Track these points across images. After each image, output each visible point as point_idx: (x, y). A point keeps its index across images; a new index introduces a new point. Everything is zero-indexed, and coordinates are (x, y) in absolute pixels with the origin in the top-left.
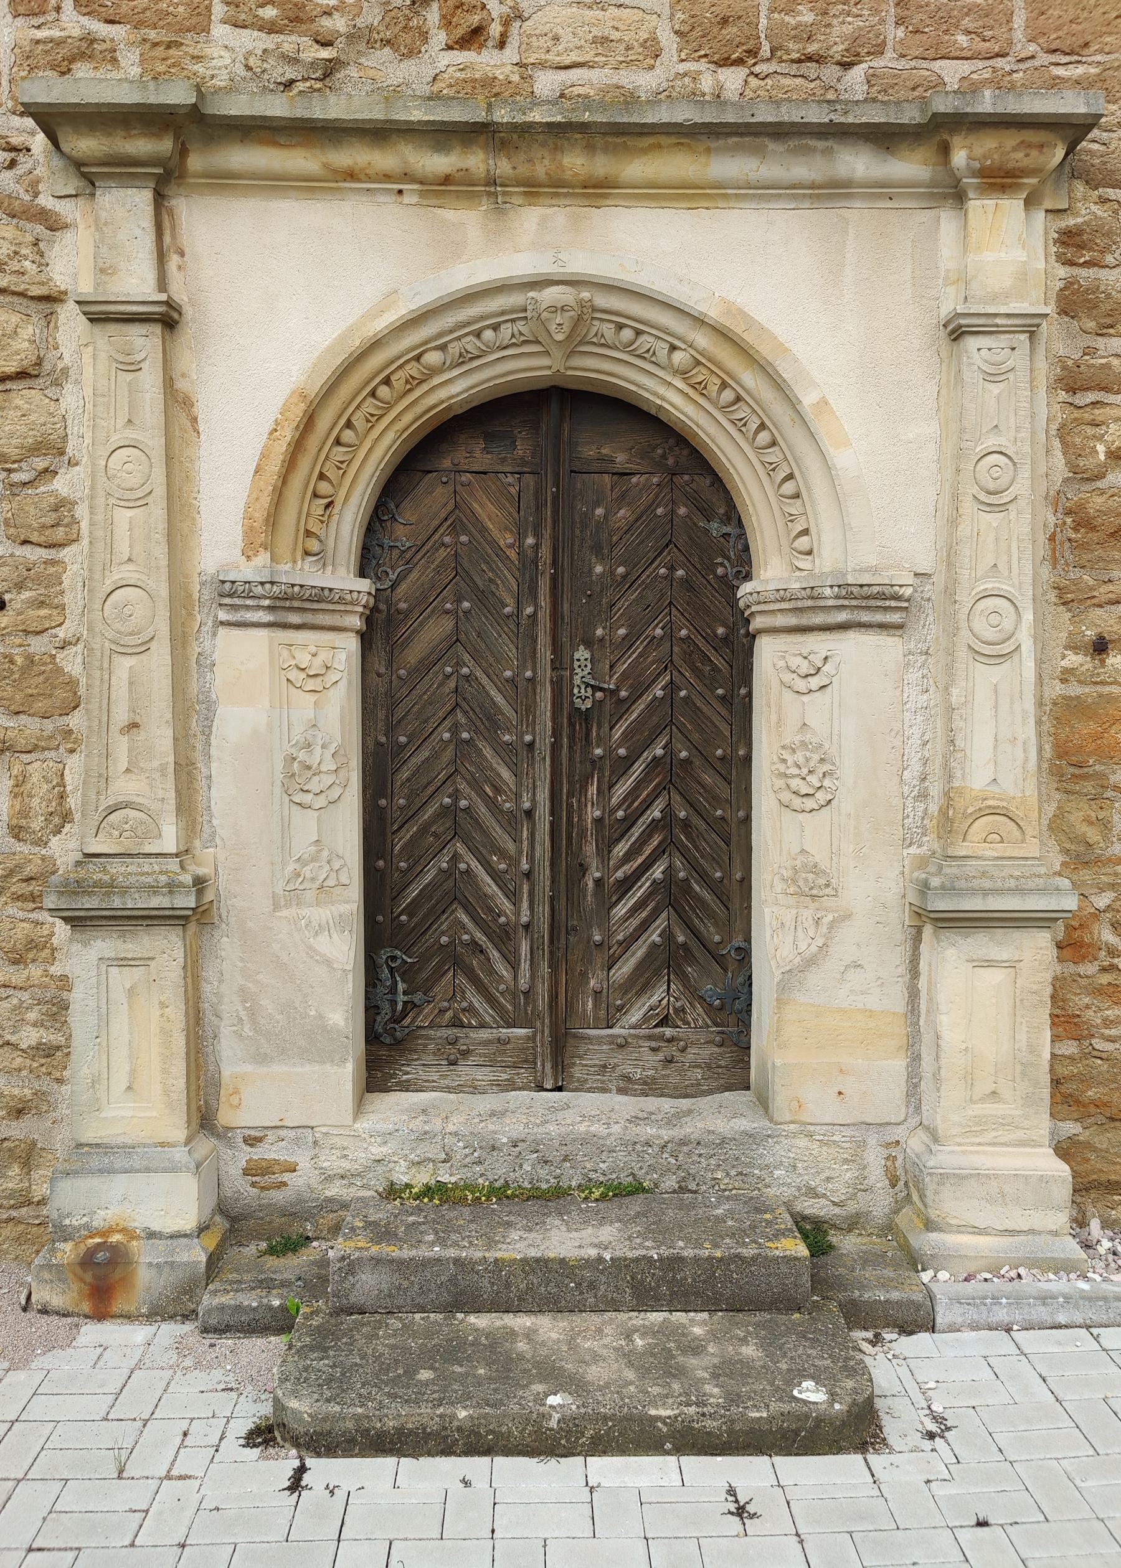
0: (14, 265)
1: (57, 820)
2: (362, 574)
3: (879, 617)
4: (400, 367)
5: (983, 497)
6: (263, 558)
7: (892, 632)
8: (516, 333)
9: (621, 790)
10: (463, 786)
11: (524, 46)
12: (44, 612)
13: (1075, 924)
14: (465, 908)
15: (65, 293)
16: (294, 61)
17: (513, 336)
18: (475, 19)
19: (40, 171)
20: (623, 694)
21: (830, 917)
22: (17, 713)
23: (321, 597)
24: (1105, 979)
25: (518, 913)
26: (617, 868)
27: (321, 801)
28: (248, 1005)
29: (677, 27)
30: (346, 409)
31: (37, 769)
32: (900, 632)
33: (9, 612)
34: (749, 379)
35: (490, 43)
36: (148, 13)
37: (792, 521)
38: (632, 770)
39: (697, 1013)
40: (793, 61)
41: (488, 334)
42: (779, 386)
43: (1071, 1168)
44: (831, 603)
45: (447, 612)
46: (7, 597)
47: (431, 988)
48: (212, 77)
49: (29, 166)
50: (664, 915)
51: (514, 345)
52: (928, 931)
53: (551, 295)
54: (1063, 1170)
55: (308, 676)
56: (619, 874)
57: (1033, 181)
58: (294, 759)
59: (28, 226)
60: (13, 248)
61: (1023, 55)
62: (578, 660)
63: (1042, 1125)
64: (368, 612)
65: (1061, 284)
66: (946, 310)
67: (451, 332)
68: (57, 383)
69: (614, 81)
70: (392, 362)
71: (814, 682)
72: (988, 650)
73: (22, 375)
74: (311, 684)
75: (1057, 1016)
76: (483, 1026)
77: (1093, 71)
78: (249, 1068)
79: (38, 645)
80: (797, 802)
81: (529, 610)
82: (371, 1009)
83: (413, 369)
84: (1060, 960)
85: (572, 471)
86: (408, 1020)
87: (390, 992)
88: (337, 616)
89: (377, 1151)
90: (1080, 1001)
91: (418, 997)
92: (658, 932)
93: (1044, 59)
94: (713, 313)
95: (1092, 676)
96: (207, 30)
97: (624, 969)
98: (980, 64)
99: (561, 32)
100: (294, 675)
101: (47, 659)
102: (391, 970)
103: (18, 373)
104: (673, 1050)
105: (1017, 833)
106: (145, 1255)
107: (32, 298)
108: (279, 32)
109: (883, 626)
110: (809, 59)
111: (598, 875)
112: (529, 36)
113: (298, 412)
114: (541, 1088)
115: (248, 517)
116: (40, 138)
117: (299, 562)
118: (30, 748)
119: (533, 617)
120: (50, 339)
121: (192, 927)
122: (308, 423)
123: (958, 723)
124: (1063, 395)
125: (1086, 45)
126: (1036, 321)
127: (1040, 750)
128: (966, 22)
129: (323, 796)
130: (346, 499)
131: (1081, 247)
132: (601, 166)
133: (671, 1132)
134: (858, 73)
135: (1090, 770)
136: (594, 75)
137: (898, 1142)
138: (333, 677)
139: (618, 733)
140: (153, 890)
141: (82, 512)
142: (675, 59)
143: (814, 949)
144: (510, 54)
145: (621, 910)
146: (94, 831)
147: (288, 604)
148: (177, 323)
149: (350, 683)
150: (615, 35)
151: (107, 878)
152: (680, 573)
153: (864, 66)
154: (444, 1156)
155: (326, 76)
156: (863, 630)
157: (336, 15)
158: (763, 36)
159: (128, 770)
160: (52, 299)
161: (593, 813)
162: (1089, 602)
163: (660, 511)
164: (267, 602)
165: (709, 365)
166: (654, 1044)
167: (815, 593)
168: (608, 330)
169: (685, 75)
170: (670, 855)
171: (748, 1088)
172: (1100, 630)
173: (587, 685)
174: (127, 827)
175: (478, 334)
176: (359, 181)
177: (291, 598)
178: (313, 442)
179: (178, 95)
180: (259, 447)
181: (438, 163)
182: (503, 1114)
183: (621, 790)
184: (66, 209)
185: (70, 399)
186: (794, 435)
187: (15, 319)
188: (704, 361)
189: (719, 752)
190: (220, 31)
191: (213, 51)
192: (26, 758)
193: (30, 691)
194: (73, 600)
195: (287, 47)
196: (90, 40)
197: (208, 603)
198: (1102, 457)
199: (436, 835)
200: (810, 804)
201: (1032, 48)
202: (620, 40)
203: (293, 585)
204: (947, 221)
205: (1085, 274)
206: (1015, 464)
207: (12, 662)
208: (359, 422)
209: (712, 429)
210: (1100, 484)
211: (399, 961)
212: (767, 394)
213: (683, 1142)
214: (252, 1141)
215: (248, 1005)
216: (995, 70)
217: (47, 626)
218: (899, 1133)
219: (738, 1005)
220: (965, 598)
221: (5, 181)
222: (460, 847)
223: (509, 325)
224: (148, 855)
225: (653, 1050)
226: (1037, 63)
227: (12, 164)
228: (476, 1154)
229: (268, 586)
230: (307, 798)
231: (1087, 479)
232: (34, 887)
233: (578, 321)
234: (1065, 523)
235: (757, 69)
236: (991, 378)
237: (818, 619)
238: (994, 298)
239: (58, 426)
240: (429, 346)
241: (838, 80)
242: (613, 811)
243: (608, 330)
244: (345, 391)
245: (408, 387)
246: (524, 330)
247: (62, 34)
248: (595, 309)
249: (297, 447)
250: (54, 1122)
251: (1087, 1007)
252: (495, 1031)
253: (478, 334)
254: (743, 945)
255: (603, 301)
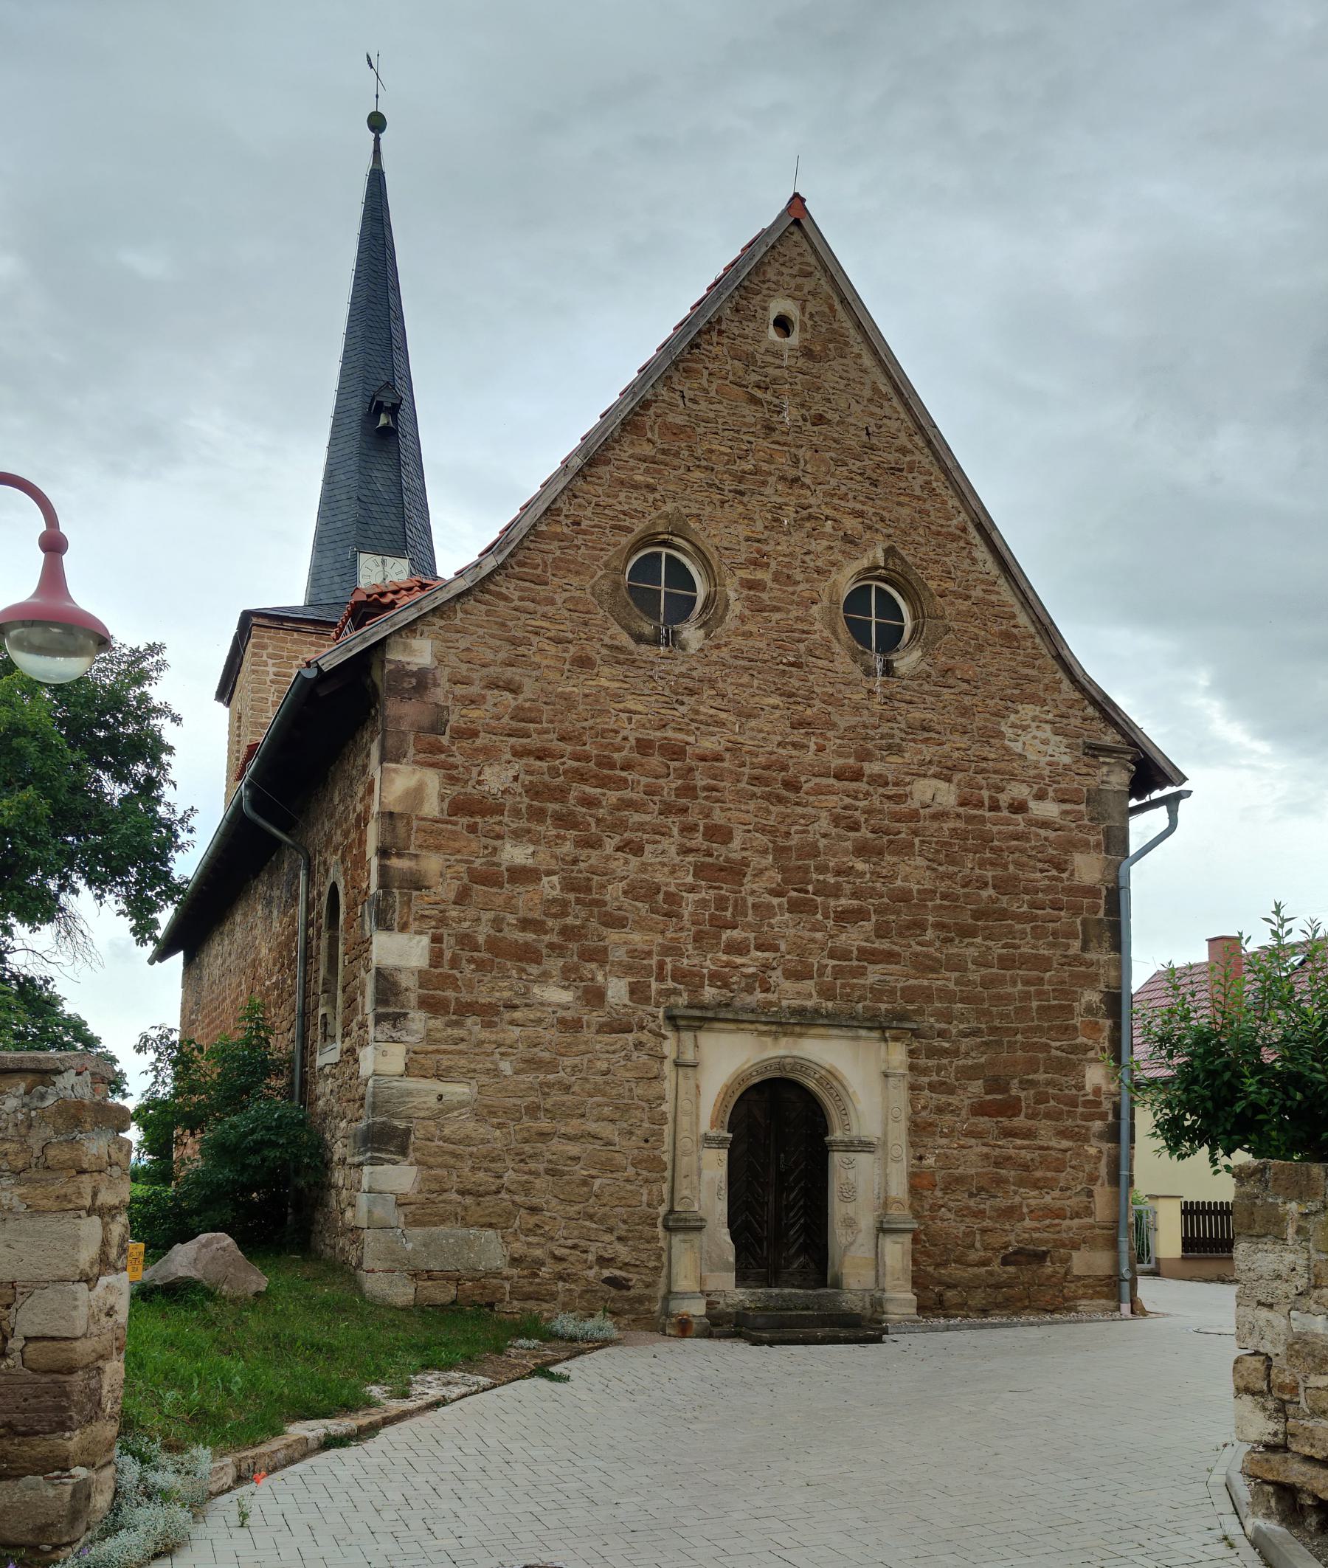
2: (729, 1132)
9: (792, 1196)
31: (655, 1187)
34: (835, 1083)
39: (812, 1265)
52: (881, 1235)
53: (788, 1060)
63: (909, 1286)
66: (883, 1068)
79: (657, 1152)
89: (742, 1298)
94: (827, 1067)
97: (793, 1251)
106: (695, 1321)
132: (804, 1030)
134: (860, 1005)
136: (797, 1002)
140: (697, 1220)
145: (792, 1233)
161: (784, 1203)
183: (792, 1196)
184: (669, 1034)
186: (847, 1099)
190: (707, 988)
196: (675, 989)
204: (883, 1045)
212: (840, 1087)
218: (873, 1292)
220: (890, 1145)
236: (895, 1088)
238: (895, 1068)
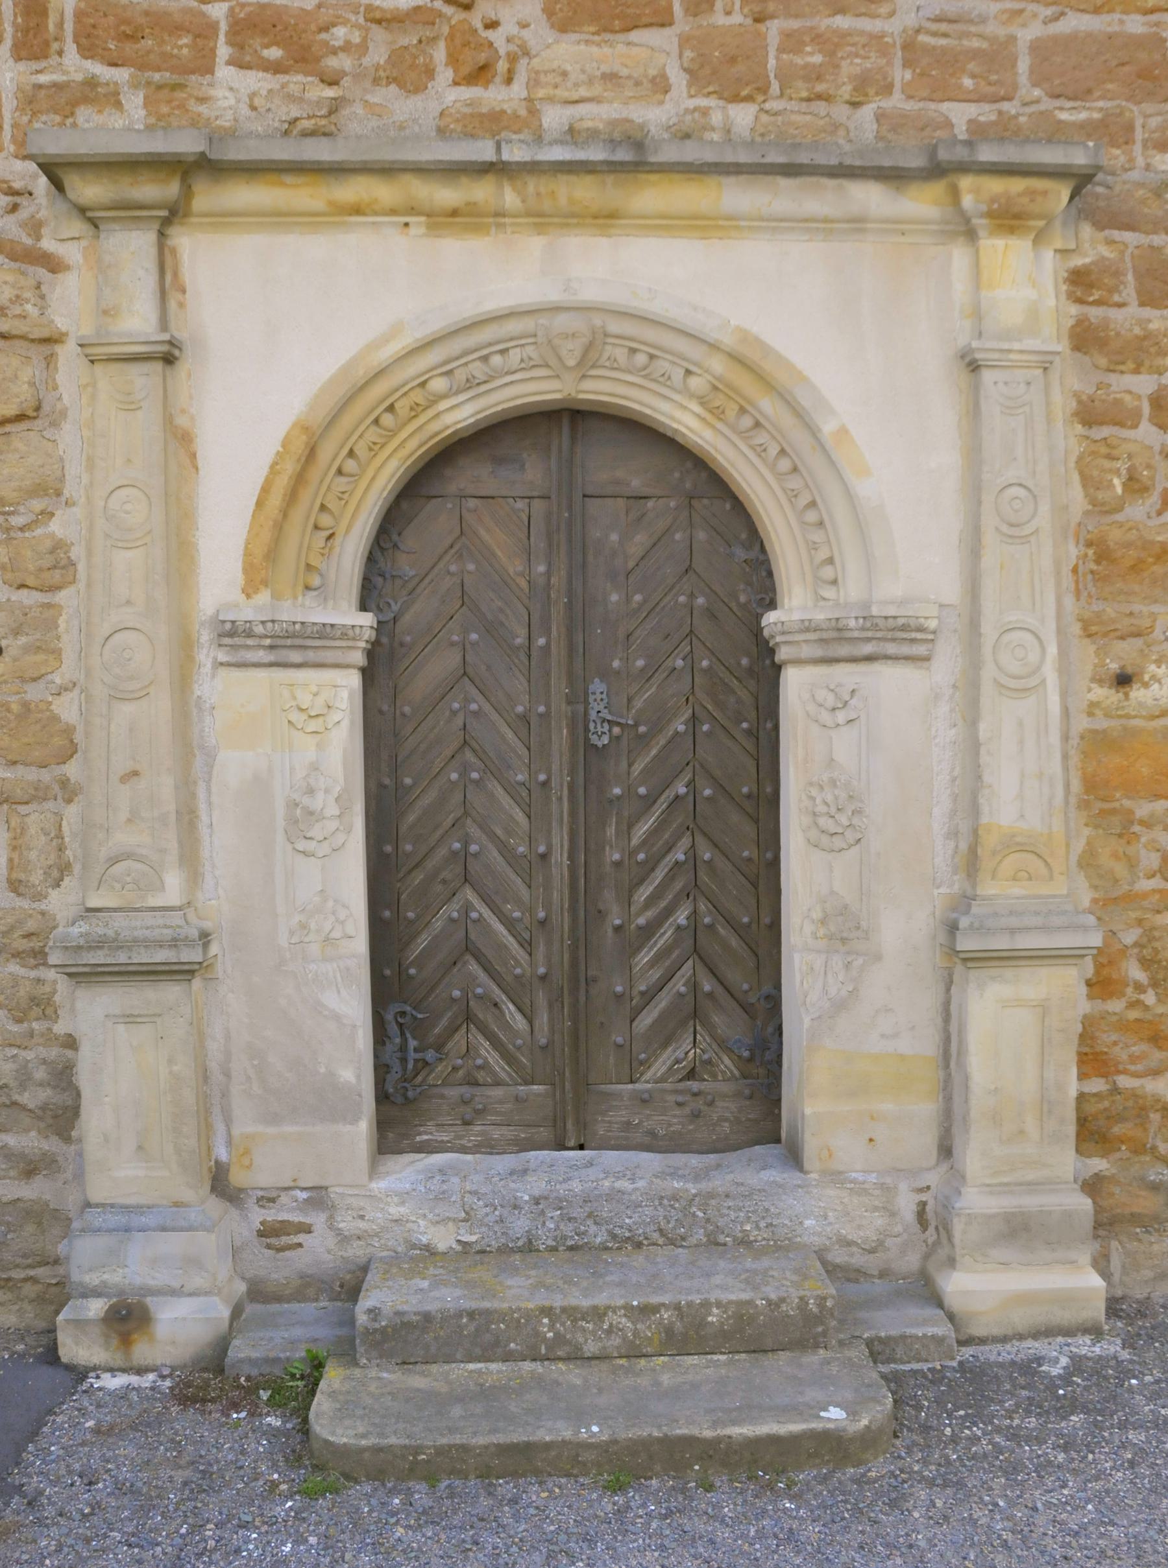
0: (17, 310)
1: (55, 873)
2: (363, 607)
3: (905, 650)
4: (405, 394)
5: (1005, 528)
6: (263, 597)
7: (919, 664)
8: (525, 356)
9: (642, 830)
10: (473, 830)
11: (532, 82)
12: (40, 657)
13: (1104, 960)
14: (477, 959)
15: (66, 334)
16: (300, 100)
17: (522, 360)
18: (482, 58)
19: (43, 214)
20: (642, 729)
21: (860, 961)
22: (15, 763)
23: (325, 632)
24: (1133, 1015)
25: (533, 964)
26: (638, 915)
27: (325, 848)
28: (255, 1062)
29: (685, 65)
30: (348, 438)
31: (36, 818)
32: (926, 664)
33: (7, 657)
34: (767, 405)
35: (498, 79)
36: (152, 56)
37: (816, 549)
38: (653, 809)
40: (802, 100)
41: (497, 360)
42: (798, 413)
43: (1094, 1203)
44: (856, 634)
45: (452, 644)
46: (4, 643)
47: (443, 1045)
48: (217, 118)
49: (32, 209)
50: (690, 962)
51: (523, 369)
53: (562, 322)
54: (1085, 1204)
55: (310, 717)
56: (641, 921)
57: (1041, 223)
58: (297, 805)
59: (31, 269)
60: (16, 292)
61: (1028, 99)
62: (594, 693)
64: (369, 646)
65: (1071, 322)
67: (457, 358)
68: (54, 424)
69: (624, 115)
70: (397, 390)
71: (841, 717)
72: (1013, 684)
73: (21, 417)
74: (312, 726)
75: (1086, 1054)
76: (498, 1083)
77: (1096, 116)
78: (260, 1128)
79: (34, 693)
80: (825, 839)
81: (542, 641)
82: (381, 1070)
83: (418, 397)
84: (1090, 997)
85: (584, 496)
86: (420, 1078)
87: (401, 1050)
88: (339, 653)
90: (1106, 1038)
91: (430, 1055)
92: (684, 980)
93: (1047, 104)
95: (1117, 709)
96: (210, 70)
97: (646, 1020)
98: (987, 107)
99: (569, 68)
100: (295, 716)
101: (43, 706)
102: (401, 1025)
103: (17, 416)
104: (699, 1103)
105: (1044, 871)
107: (33, 341)
108: (285, 71)
109: (907, 658)
110: (819, 97)
111: (618, 922)
112: (537, 73)
113: (299, 446)
114: (562, 1147)
115: (247, 553)
116: (43, 180)
117: (300, 598)
118: (26, 798)
119: (546, 649)
120: (50, 381)
121: (197, 983)
122: (311, 453)
123: (984, 758)
124: (1079, 428)
125: (1089, 91)
126: (1049, 358)
127: (1067, 786)
128: (971, 66)
129: (326, 844)
130: (348, 531)
131: (1091, 286)
133: (699, 1186)
135: (1116, 805)
137: (928, 1188)
138: (336, 716)
139: (638, 768)
141: (77, 552)
142: (685, 95)
143: (844, 993)
144: (518, 89)
146: (96, 884)
147: (289, 642)
148: (176, 358)
149: (352, 723)
150: (625, 72)
151: (111, 933)
152: (701, 600)
153: (873, 106)
154: (463, 1215)
155: (330, 113)
156: (890, 662)
157: (341, 55)
158: (772, 75)
159: (129, 820)
160: (52, 340)
162: (1112, 635)
163: (678, 536)
164: (268, 642)
165: (726, 390)
166: (680, 1099)
167: (840, 625)
168: (621, 354)
169: (695, 109)
170: (695, 899)
171: (778, 1141)
172: (1122, 663)
173: (604, 720)
174: (128, 879)
175: (485, 359)
176: (364, 214)
177: (293, 636)
178: (314, 474)
179: (187, 144)
180: (261, 480)
181: (446, 195)
182: (525, 1172)
183: (642, 830)
185: (68, 439)
187: (15, 362)
188: (721, 387)
189: (745, 790)
190: (224, 72)
191: (219, 93)
192: (23, 809)
193: (26, 740)
194: (68, 644)
195: (293, 88)
196: (91, 83)
197: (207, 645)
198: (1119, 490)
199: (444, 882)
200: (838, 842)
201: (1037, 92)
202: (629, 77)
203: (294, 623)
204: (959, 256)
205: (1095, 313)
206: (1035, 497)
207: (9, 710)
208: (361, 451)
209: (730, 453)
210: (1119, 517)
211: (408, 1018)
212: (786, 420)
213: (711, 1195)
214: (267, 1200)
215: (255, 1062)
216: (1000, 113)
217: (43, 672)
219: (769, 1055)
221: (10, 227)
222: (470, 894)
223: (518, 350)
224: (154, 909)
225: (679, 1104)
226: (1042, 107)
227: (14, 208)
228: (497, 1213)
229: (270, 625)
230: (311, 846)
231: (1106, 512)
232: (35, 944)
233: (589, 348)
234: (1086, 555)
235: (767, 106)
237: (844, 650)
239: (56, 466)
240: (435, 373)
241: (848, 118)
242: (633, 853)
243: (621, 354)
244: (348, 420)
245: (413, 414)
246: (534, 355)
247: (65, 78)
248: (606, 335)
249: (300, 479)
250: (65, 1183)
251: (1115, 1043)
252: (511, 1088)
253: (485, 359)
254: (773, 992)
255: (614, 327)
